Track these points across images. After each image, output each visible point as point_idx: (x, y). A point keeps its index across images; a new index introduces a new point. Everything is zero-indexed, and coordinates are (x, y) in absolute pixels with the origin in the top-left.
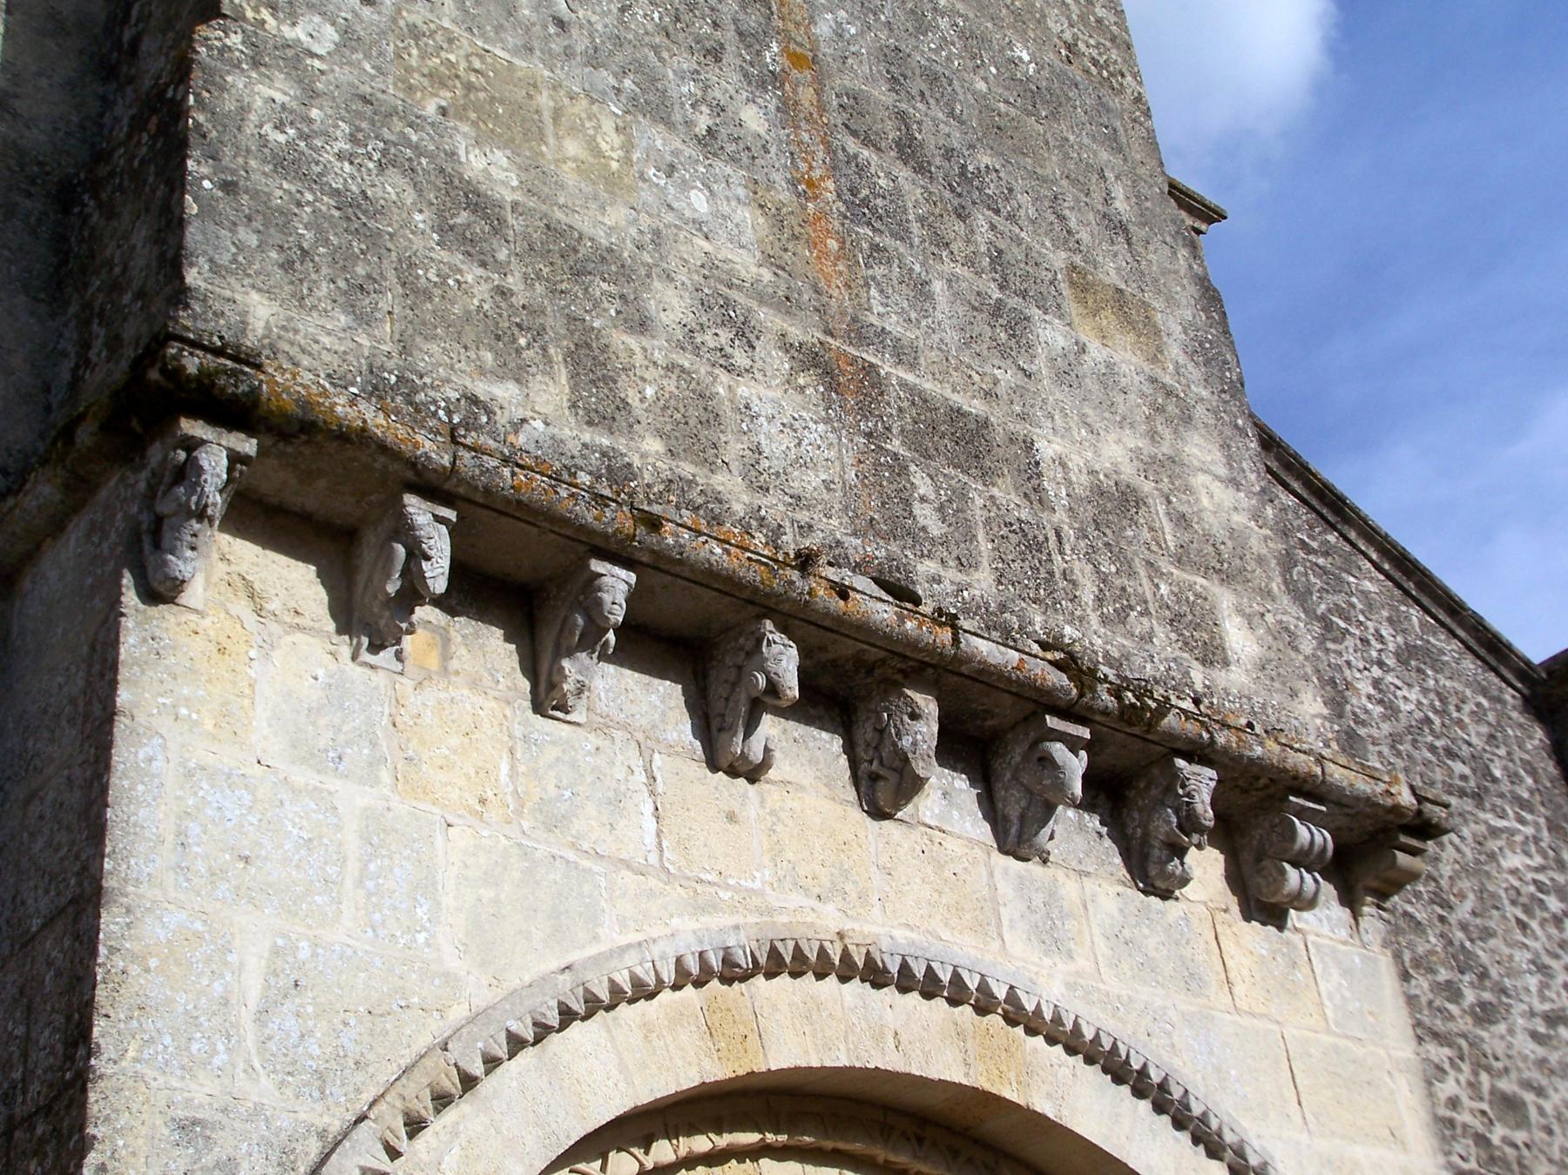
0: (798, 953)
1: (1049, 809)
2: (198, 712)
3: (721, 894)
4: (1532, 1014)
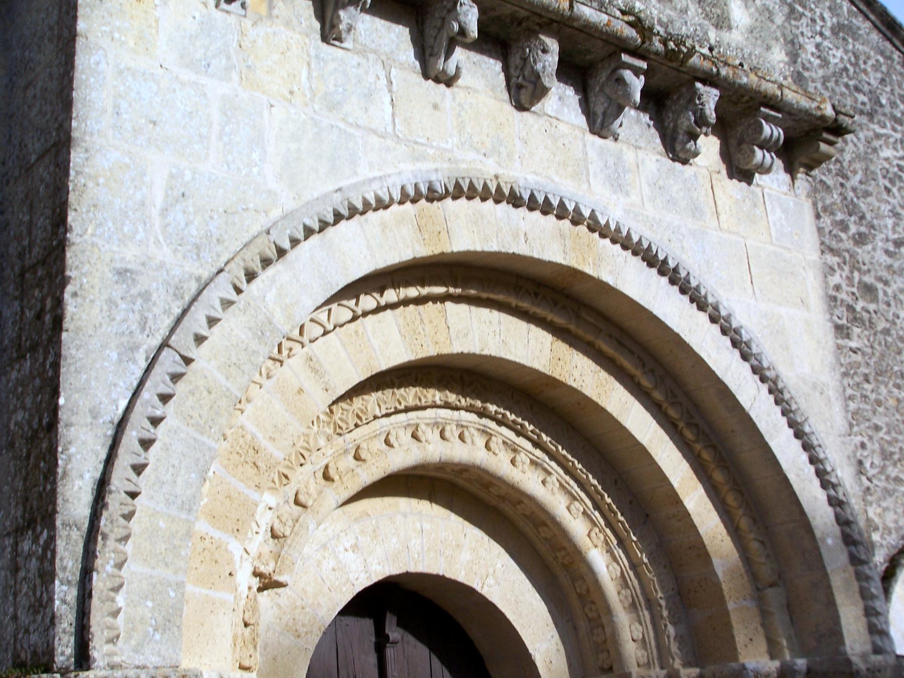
0: (472, 186)
1: (620, 109)
2: (125, 36)
3: (428, 150)
4: (887, 240)
